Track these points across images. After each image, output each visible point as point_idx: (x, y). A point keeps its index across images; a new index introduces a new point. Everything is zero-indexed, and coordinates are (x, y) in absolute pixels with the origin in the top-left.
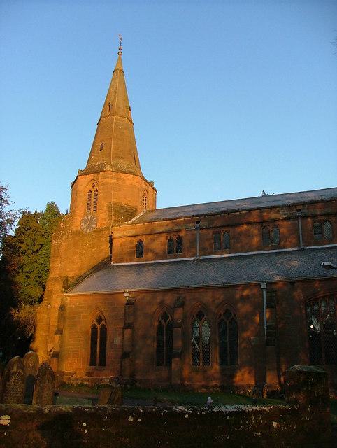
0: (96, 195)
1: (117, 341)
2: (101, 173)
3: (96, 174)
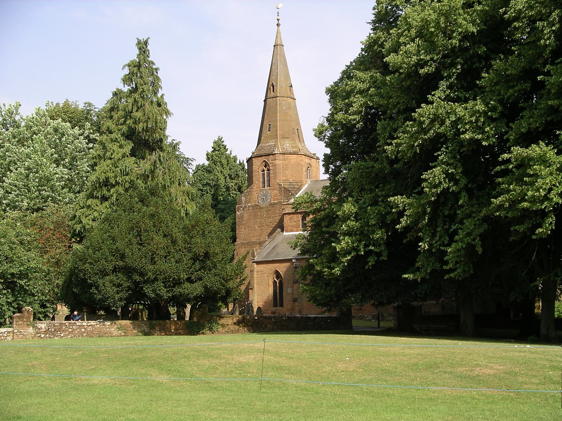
0: (269, 174)
1: (289, 290)
2: (271, 156)
3: (267, 157)
